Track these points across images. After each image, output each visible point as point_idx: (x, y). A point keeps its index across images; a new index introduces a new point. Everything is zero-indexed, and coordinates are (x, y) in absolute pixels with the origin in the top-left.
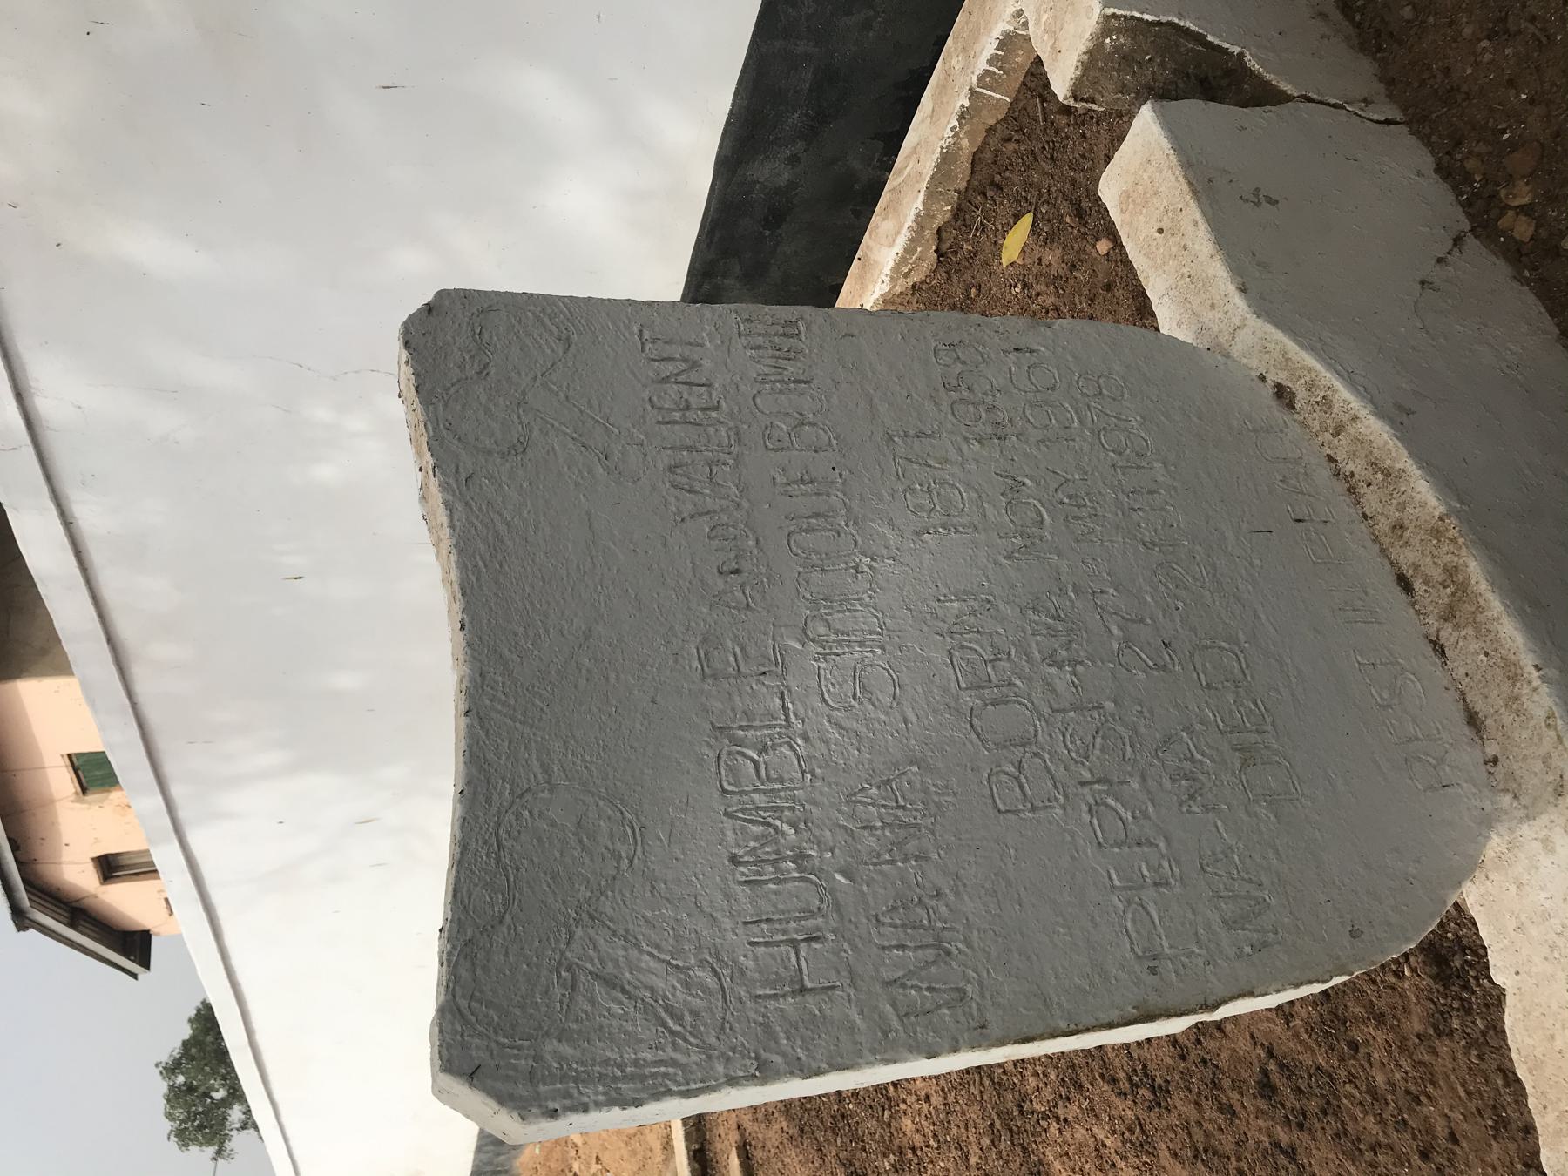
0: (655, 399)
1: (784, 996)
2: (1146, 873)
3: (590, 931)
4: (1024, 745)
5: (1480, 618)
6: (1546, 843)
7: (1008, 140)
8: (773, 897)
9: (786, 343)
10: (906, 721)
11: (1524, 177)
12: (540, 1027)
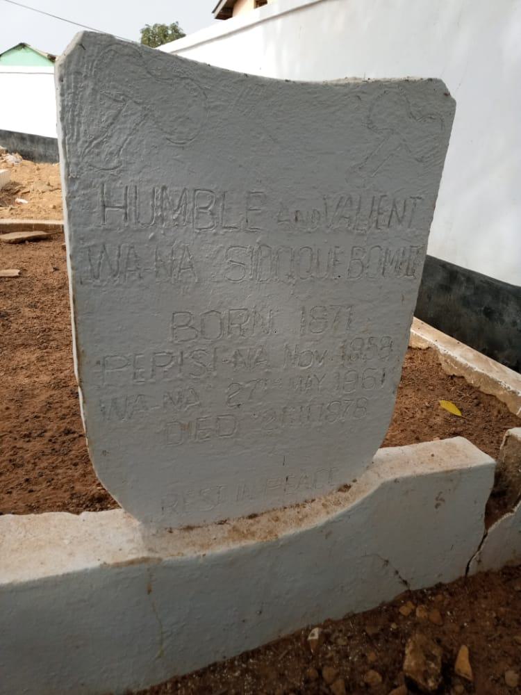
0: (386, 198)
1: (102, 197)
2: (140, 370)
3: (139, 114)
4: (202, 331)
5: (231, 540)
6: (132, 541)
7: (499, 412)
8: (146, 202)
9: (404, 268)
10: (218, 282)
11: (428, 615)
12: (99, 81)
